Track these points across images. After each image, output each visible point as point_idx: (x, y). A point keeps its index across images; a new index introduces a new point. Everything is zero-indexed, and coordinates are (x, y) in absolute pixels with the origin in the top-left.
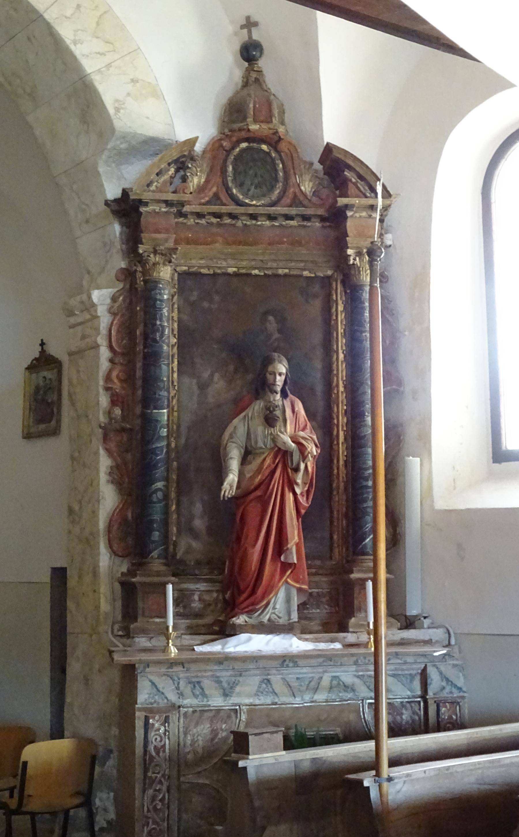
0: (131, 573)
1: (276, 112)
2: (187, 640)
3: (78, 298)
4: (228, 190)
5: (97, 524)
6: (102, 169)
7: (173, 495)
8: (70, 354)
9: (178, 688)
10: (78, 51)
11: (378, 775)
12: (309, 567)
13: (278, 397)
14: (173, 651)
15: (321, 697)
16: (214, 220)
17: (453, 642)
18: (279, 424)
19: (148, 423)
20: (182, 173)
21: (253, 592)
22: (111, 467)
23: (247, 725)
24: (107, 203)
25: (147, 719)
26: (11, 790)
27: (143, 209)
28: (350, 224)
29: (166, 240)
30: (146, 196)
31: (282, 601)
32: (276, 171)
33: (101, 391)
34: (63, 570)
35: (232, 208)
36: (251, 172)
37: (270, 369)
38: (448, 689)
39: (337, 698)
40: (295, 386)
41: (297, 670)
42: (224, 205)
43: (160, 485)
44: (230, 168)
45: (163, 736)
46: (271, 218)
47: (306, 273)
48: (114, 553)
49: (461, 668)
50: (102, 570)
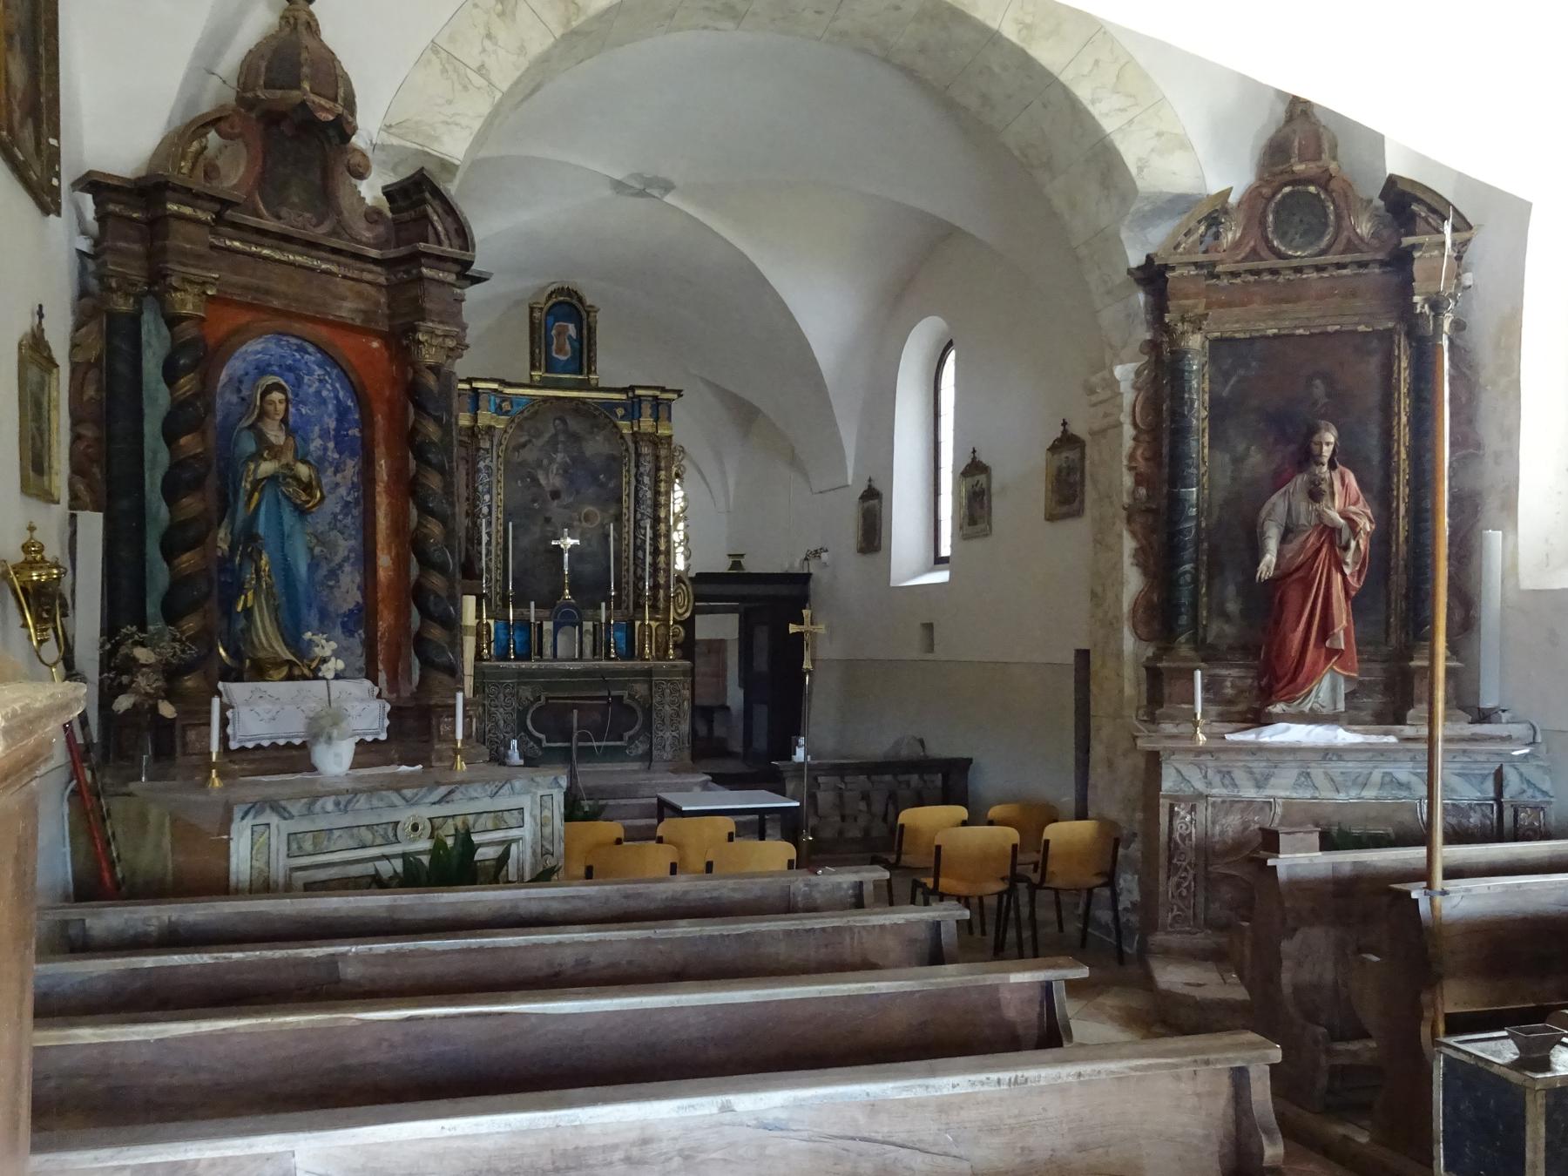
0: (1157, 657)
1: (1326, 146)
2: (1218, 727)
3: (1100, 375)
4: (1267, 241)
5: (1121, 608)
6: (1123, 236)
7: (1203, 577)
8: (1092, 433)
9: (1205, 777)
10: (1095, 110)
11: (1429, 887)
12: (1359, 652)
13: (1325, 468)
14: (1202, 738)
15: (1369, 794)
16: (1251, 278)
17: (1539, 739)
18: (1326, 500)
19: (1175, 503)
20: (1214, 229)
21: (1293, 679)
22: (1136, 550)
23: (1280, 824)
24: (1130, 271)
25: (1172, 807)
26: (1036, 865)
27: (1169, 275)
28: (1417, 268)
29: (1195, 306)
30: (1171, 261)
31: (1326, 689)
32: (1326, 215)
33: (1125, 470)
34: (1087, 652)
35: (1281, 263)
36: (1297, 219)
37: (1316, 438)
38: (1530, 792)
39: (1389, 796)
40: (1343, 457)
41: (1342, 764)
42: (1262, 259)
43: (1188, 567)
44: (1271, 218)
45: (1189, 824)
46: (1319, 268)
47: (1361, 328)
48: (1139, 637)
49: (1547, 770)
50: (1126, 653)
